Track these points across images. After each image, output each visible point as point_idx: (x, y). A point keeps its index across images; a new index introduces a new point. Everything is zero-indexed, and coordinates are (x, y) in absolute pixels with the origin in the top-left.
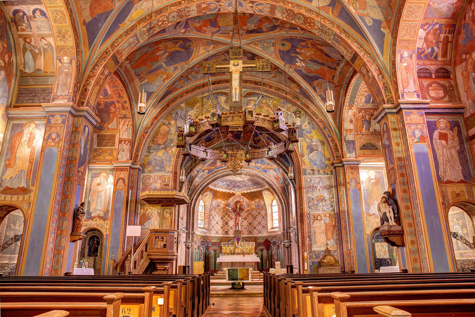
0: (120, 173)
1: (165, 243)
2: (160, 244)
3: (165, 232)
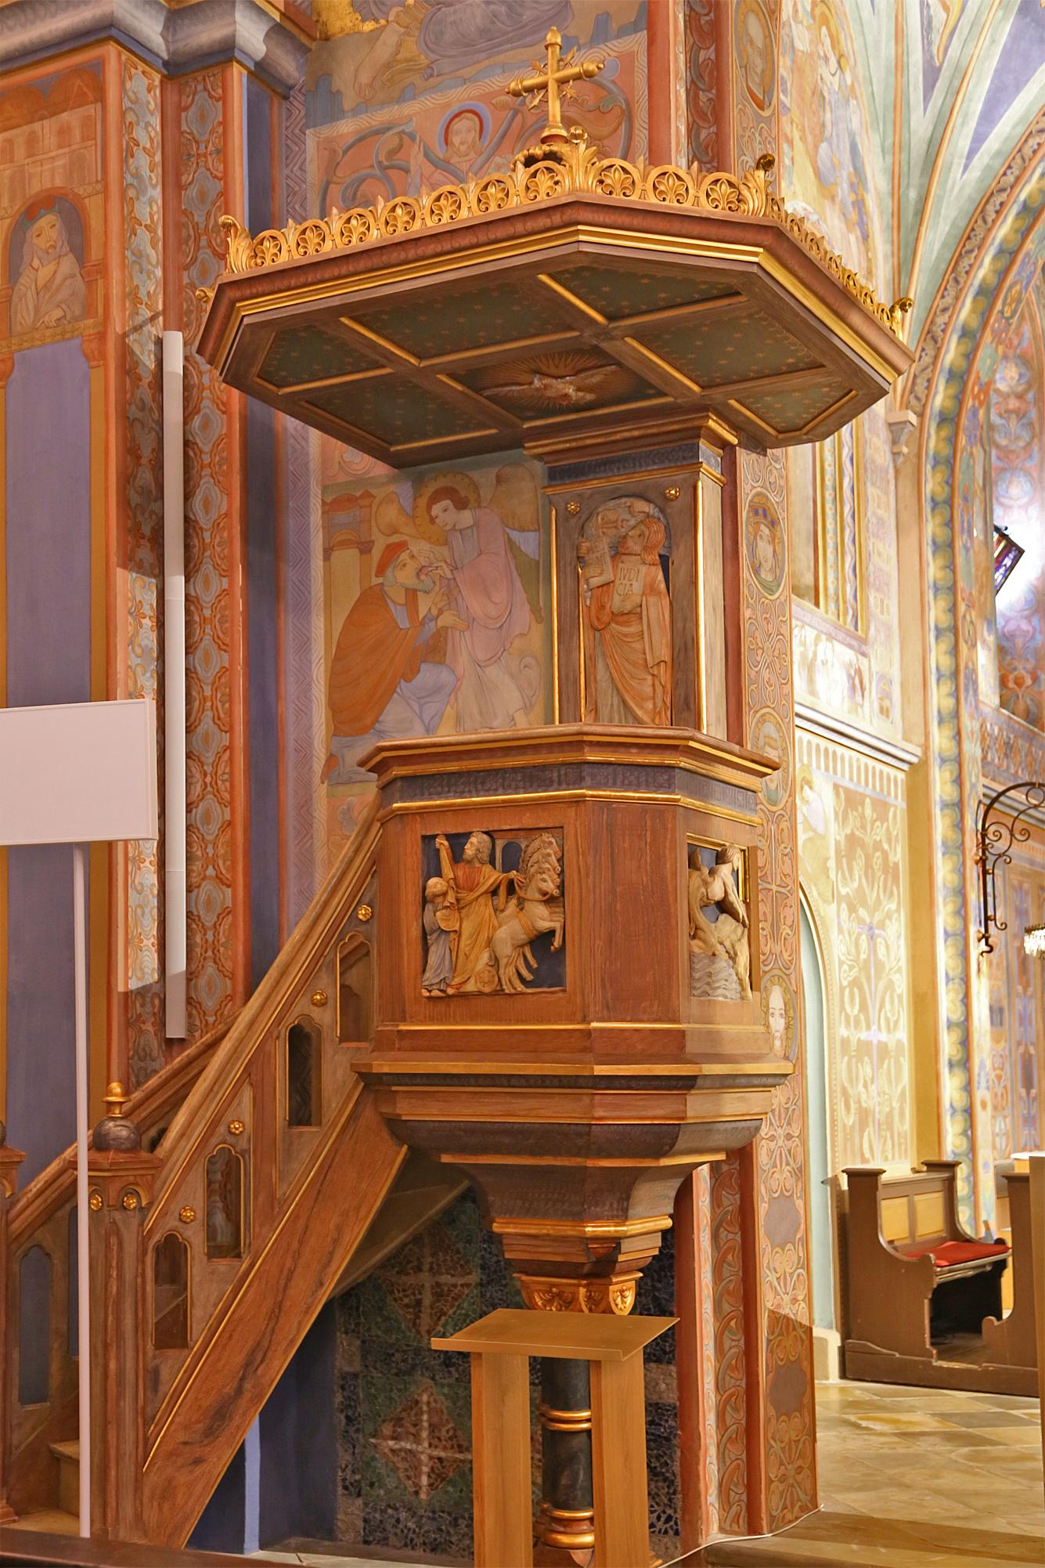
0: (32, 141)
1: (543, 918)
2: (488, 939)
3: (535, 777)
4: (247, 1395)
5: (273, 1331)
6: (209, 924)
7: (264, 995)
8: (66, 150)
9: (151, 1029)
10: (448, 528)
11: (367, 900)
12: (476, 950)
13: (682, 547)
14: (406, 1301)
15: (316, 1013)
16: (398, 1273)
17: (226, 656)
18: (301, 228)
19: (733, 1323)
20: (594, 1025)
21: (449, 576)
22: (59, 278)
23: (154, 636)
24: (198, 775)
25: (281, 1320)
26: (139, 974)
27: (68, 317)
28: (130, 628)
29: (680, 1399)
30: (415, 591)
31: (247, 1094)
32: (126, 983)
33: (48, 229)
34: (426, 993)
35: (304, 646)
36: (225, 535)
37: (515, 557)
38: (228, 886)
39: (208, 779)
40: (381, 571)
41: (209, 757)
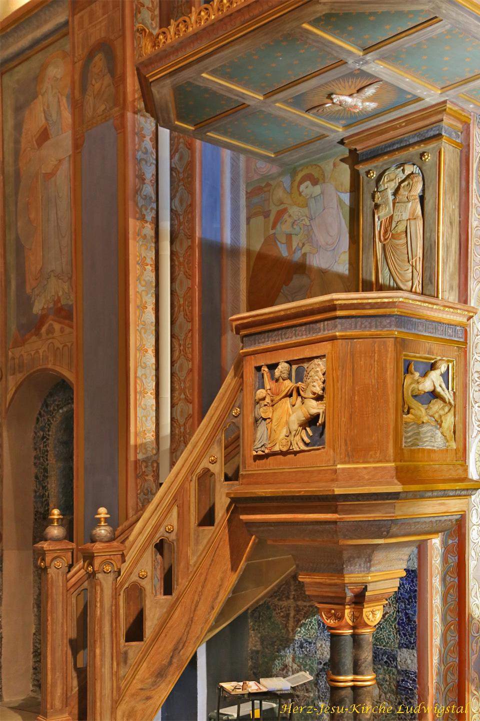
1: (315, 407)
4: (174, 665)
5: (188, 632)
6: (182, 423)
7: (184, 459)
8: (106, 16)
9: (152, 479)
10: (308, 197)
11: (237, 404)
12: (280, 428)
13: (431, 189)
14: (282, 614)
15: (212, 467)
16: (278, 600)
17: (190, 282)
18: (177, 23)
19: (452, 627)
20: (339, 466)
21: (308, 224)
22: (104, 87)
23: (153, 275)
24: (177, 346)
25: (193, 626)
26: (144, 451)
27: (108, 108)
28: (138, 272)
29: (418, 668)
30: (291, 235)
31: (175, 511)
32: (136, 456)
33: (99, 60)
34: (255, 453)
35: (236, 274)
36: (190, 216)
37: (342, 208)
38: (191, 403)
39: (182, 348)
40: (274, 227)
41: (182, 336)
